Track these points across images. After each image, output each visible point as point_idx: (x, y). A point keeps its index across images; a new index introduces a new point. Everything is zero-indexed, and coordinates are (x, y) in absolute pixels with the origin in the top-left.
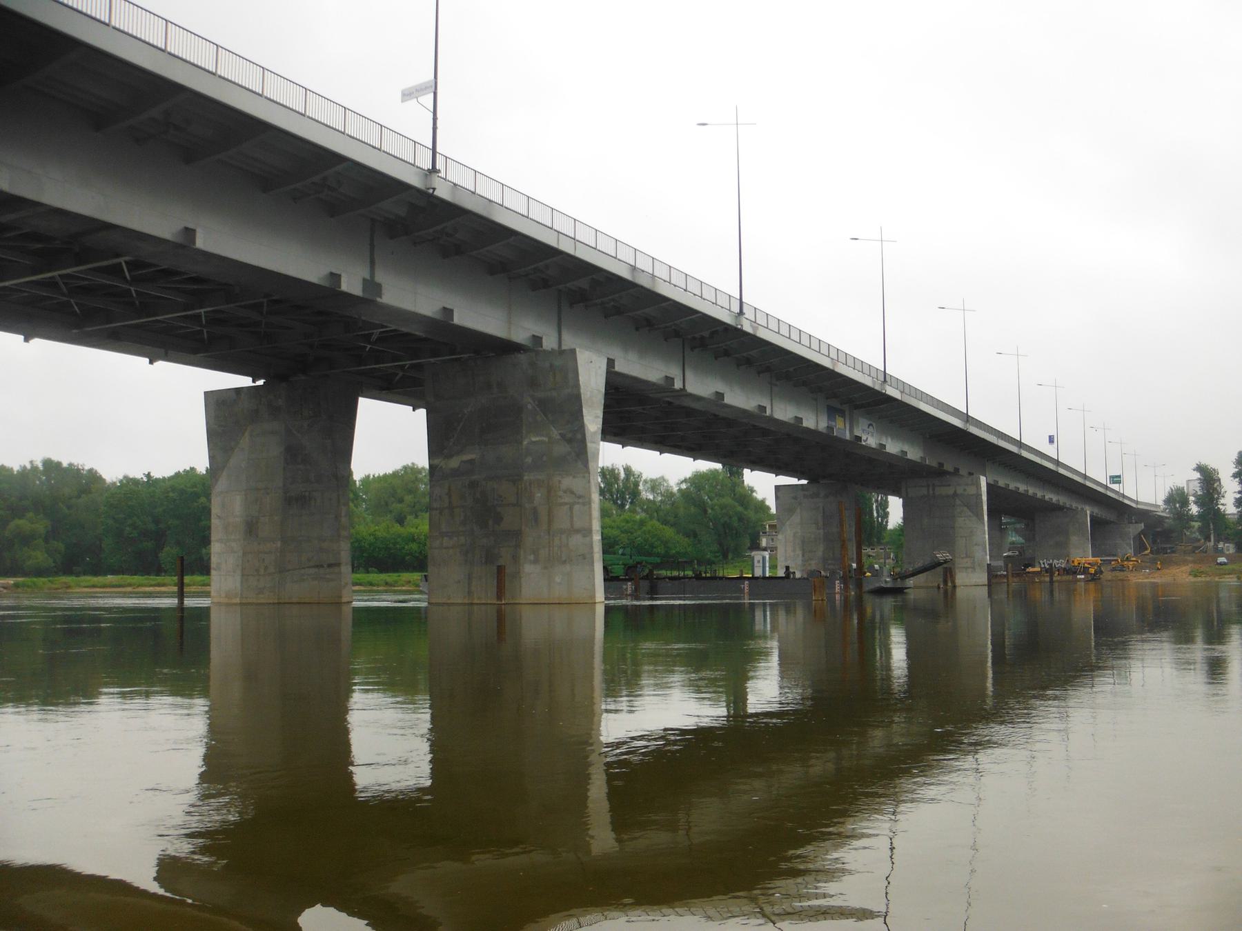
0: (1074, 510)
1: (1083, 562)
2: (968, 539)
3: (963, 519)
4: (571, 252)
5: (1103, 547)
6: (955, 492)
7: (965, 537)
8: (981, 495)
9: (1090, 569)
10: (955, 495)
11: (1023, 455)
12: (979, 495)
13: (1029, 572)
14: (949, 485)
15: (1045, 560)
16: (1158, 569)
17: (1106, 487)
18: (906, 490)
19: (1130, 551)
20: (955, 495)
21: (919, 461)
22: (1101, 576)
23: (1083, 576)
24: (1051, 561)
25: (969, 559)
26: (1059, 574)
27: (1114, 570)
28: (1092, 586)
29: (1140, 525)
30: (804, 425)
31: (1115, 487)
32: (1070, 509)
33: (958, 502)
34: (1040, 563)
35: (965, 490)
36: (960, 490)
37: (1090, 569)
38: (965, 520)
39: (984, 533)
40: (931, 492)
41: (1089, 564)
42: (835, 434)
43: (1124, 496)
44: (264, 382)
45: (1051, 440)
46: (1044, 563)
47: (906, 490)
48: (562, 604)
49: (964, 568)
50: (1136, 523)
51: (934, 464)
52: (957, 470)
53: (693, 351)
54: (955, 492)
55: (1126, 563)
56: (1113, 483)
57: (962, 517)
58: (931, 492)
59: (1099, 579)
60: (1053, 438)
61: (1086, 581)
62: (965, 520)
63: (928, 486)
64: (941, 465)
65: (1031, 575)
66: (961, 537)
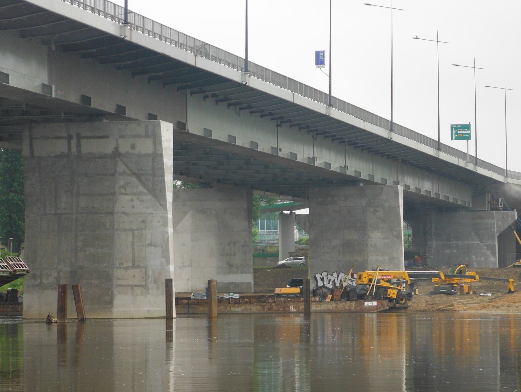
0: (377, 184)
1: (377, 277)
2: (136, 233)
3: (129, 197)
4: (416, 148)
5: (447, 251)
6: (117, 148)
7: (133, 230)
8: (161, 155)
9: (389, 291)
10: (116, 154)
11: (394, 139)
12: (158, 156)
13: (279, 295)
14: (107, 137)
15: (324, 274)
16: (510, 291)
17: (439, 146)
18: (31, 144)
19: (492, 259)
20: (116, 154)
21: (39, 91)
22: (409, 303)
23: (375, 303)
24: (335, 275)
25: (137, 271)
26: (332, 300)
27: (436, 292)
28: (393, 319)
29: (510, 213)
30: (213, 137)
31: (460, 145)
32: (370, 183)
33: (121, 167)
34: (316, 279)
35: (133, 147)
36: (124, 147)
37: (389, 291)
38: (132, 200)
39: (165, 225)
40: (74, 149)
41: (389, 281)
42: (54, 96)
43: (476, 161)
44: (290, 212)
45: (320, 60)
46: (322, 279)
47: (31, 144)
48: (134, 318)
49: (129, 285)
50: (505, 209)
51: (73, 98)
52: (121, 110)
53: (261, 118)
54: (117, 148)
55: (457, 280)
56: (457, 139)
57: (126, 194)
58: (74, 149)
59: (406, 308)
60: (324, 56)
61: (381, 312)
62: (132, 200)
63: (69, 138)
64: (86, 100)
65: (282, 299)
66: (125, 230)
